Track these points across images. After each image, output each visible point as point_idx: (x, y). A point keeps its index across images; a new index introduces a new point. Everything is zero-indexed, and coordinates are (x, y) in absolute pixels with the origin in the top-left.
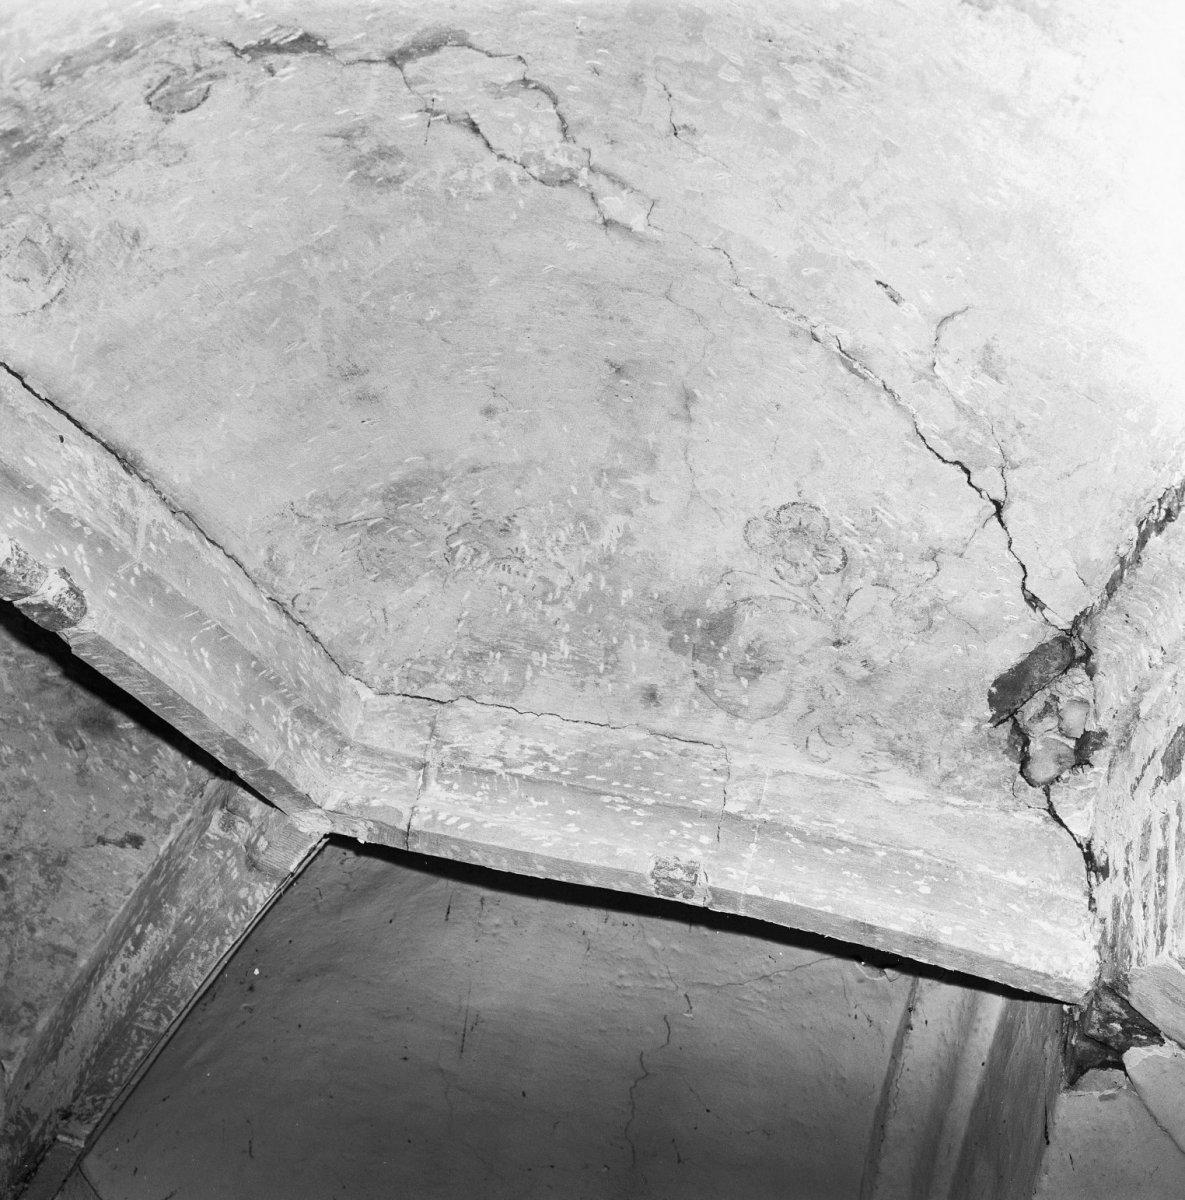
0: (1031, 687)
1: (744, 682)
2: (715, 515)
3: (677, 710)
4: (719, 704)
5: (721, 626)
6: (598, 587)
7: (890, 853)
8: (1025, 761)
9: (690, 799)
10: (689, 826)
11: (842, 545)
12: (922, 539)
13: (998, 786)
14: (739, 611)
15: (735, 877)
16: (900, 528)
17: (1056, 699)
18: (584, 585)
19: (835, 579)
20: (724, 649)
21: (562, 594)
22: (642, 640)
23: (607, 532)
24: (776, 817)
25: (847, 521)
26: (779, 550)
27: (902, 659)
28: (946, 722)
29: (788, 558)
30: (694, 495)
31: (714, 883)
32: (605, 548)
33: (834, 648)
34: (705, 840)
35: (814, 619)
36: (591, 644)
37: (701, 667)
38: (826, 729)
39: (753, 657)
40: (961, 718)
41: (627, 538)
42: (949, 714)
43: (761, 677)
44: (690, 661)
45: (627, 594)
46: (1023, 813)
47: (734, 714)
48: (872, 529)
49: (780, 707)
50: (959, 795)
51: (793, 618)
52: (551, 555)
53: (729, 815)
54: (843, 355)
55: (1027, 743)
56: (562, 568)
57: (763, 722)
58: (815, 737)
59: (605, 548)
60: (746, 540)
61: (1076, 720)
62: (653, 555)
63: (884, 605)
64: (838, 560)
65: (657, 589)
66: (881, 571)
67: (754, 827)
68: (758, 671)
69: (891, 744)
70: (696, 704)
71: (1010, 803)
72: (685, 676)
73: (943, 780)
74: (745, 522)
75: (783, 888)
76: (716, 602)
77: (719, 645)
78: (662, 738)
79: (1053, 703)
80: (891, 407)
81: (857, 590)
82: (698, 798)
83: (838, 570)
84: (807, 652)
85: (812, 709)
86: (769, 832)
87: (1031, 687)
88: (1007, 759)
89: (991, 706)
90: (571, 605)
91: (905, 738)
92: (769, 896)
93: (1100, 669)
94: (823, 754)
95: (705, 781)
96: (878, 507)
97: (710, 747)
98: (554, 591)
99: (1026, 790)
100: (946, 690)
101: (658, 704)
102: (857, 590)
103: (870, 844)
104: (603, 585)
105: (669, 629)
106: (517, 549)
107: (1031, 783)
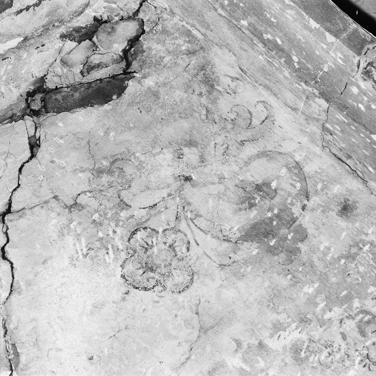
0: (88, 89)
1: (274, 185)
2: (200, 309)
3: (336, 189)
4: (303, 178)
5: (258, 232)
6: (326, 305)
7: (238, 20)
8: (134, 41)
9: (349, 124)
10: (360, 106)
11: (127, 243)
12: (71, 221)
13: (165, 31)
14: (238, 235)
15: (339, 55)
16: (79, 235)
17: (82, 73)
18: (337, 312)
19: (152, 224)
20: (269, 215)
21: (357, 315)
22: (323, 252)
23: (289, 339)
24: (298, 82)
25: (110, 258)
26: (175, 263)
27: (153, 147)
28: (162, 90)
29: (173, 254)
30: (204, 330)
31: (354, 57)
32: (299, 330)
33: (194, 178)
34: (355, 90)
35: (189, 204)
36: (361, 269)
37: (296, 210)
38: (242, 123)
39: (254, 198)
40: (149, 88)
41: (278, 327)
42: (155, 95)
43: (260, 182)
44: (300, 218)
45: (310, 290)
46: (162, 5)
47: (298, 166)
48: (98, 244)
49: (263, 154)
50: (193, 36)
51: (202, 212)
52: (344, 346)
53: (327, 100)
54: (13, 368)
55: (125, 52)
56: (342, 334)
57: (282, 150)
58: (256, 122)
59: (299, 330)
60: (192, 280)
61: (78, 52)
62: (269, 306)
63: (134, 189)
64: (139, 235)
65: (284, 282)
66: (117, 213)
67: (316, 82)
68: (258, 188)
69: (210, 93)
70: (319, 186)
71: (165, 16)
72: (313, 210)
73: (195, 51)
74: (183, 294)
75: (311, 31)
76: (252, 249)
77: (271, 219)
78: (360, 175)
79: (85, 70)
80: (13, 318)
81: (144, 208)
82: (344, 122)
83: (145, 228)
84: (213, 184)
85: (242, 143)
86: (310, 74)
87: (88, 89)
88: (145, 47)
89: (125, 88)
90: (356, 304)
91: (196, 93)
92: (322, 29)
93: (32, 80)
94: (260, 107)
95: (338, 130)
96: (81, 257)
97: (332, 151)
98: (361, 321)
99: (148, 20)
100: (143, 112)
101: (346, 200)
102: (144, 208)
103: (247, 32)
104: (322, 305)
105: (298, 249)
106: (364, 366)
107: (142, 23)
